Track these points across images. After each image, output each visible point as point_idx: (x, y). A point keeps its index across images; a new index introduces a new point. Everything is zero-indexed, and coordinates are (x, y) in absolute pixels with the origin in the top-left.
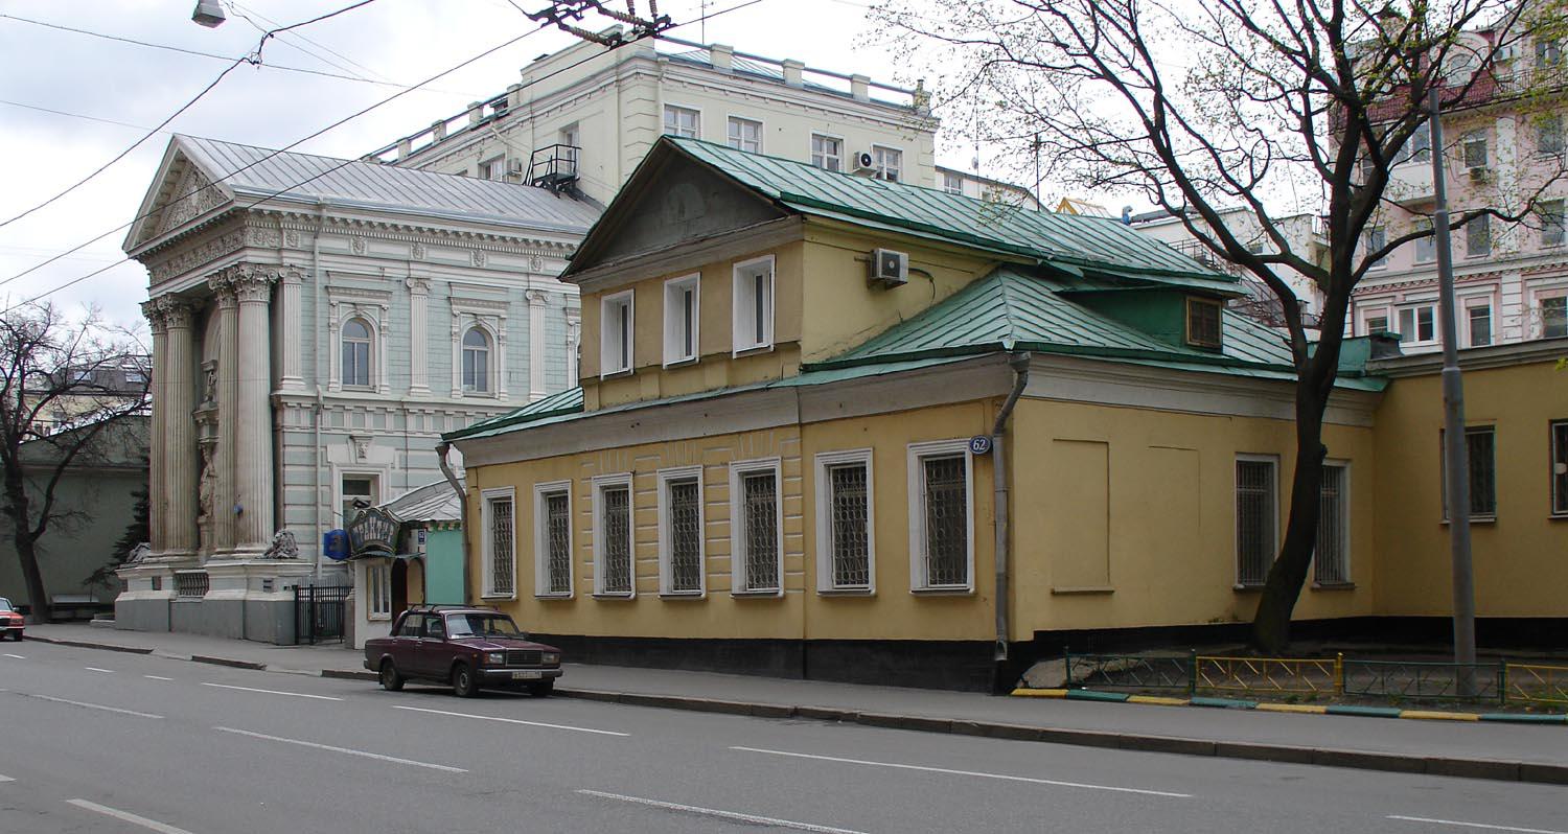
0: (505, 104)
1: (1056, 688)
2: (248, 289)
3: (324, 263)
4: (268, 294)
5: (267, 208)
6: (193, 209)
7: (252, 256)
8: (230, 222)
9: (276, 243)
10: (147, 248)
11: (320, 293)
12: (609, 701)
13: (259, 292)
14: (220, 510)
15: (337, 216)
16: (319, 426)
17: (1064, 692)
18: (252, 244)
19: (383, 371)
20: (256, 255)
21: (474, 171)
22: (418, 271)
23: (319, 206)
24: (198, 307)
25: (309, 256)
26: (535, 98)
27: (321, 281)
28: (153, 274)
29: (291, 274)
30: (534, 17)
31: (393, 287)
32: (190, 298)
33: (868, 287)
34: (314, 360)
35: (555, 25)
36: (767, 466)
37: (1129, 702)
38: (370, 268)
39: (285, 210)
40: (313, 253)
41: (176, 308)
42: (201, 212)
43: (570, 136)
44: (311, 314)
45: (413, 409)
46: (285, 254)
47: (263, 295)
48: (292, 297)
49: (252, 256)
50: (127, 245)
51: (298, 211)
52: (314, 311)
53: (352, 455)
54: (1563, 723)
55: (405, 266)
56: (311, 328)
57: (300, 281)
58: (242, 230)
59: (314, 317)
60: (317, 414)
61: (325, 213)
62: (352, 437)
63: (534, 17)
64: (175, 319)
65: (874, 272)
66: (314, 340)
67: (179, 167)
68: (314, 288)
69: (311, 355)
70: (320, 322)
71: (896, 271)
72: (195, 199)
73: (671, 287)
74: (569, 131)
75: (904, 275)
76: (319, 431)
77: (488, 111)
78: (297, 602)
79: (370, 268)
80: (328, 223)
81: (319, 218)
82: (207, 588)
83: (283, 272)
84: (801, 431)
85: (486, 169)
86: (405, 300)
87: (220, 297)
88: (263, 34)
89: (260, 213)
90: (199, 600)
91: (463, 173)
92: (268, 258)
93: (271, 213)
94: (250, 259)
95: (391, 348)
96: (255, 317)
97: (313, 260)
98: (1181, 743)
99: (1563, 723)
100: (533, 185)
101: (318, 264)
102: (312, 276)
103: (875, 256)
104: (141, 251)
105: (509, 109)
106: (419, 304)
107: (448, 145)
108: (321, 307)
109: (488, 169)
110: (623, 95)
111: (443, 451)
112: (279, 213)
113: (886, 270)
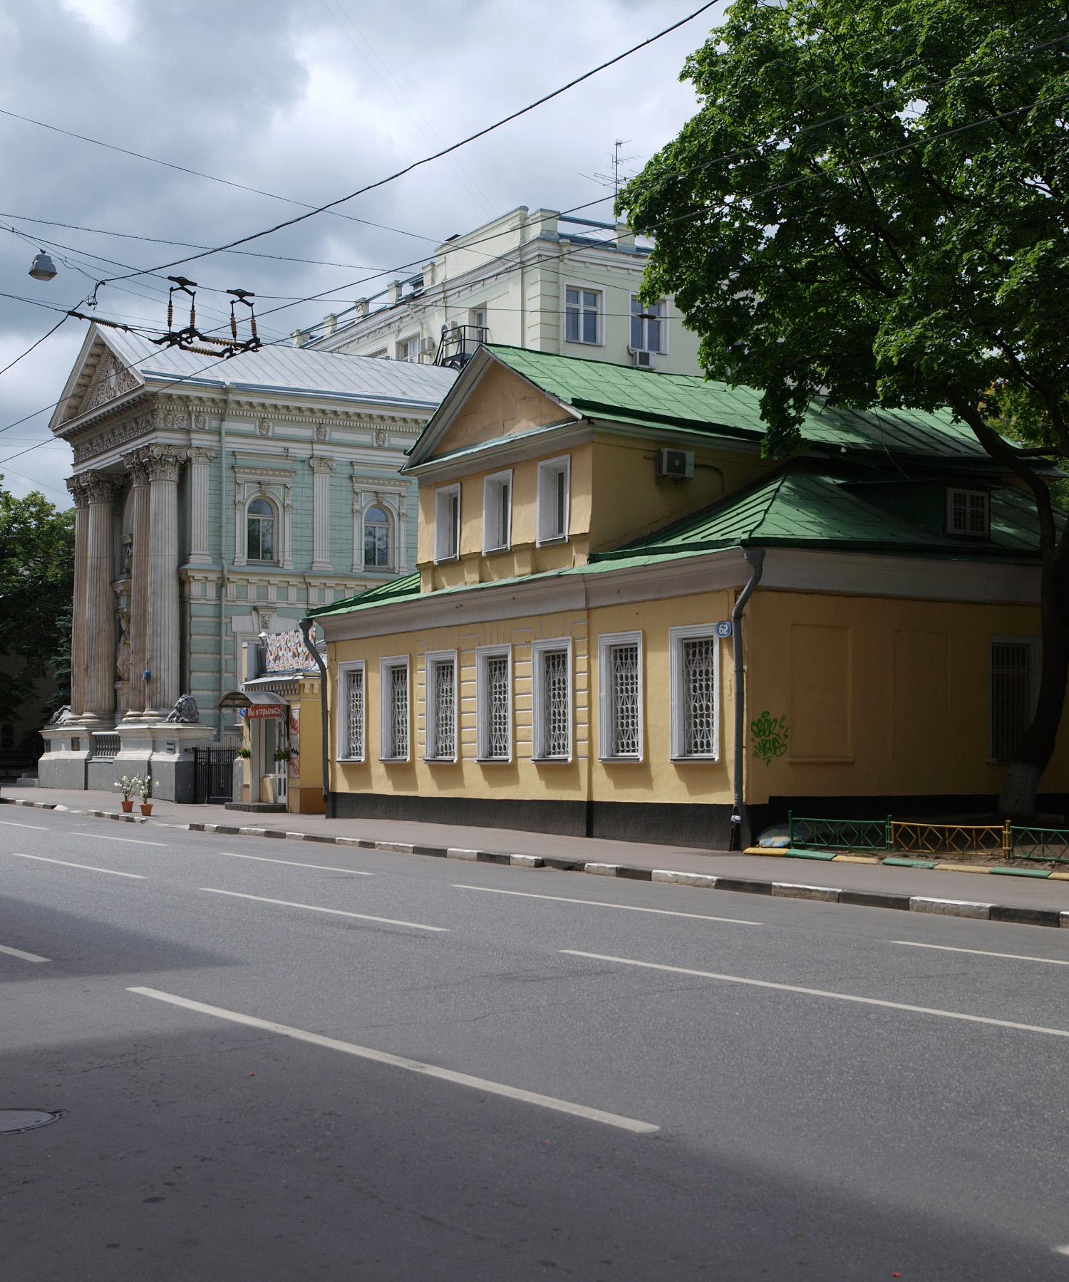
0: (421, 283)
2: (158, 468)
3: (231, 444)
5: (174, 391)
6: (112, 393)
7: (162, 437)
8: (142, 407)
9: (185, 424)
10: (70, 427)
11: (226, 473)
12: (751, 884)
14: (134, 673)
15: (243, 399)
17: (784, 851)
18: (162, 425)
19: (287, 549)
21: (392, 352)
22: (320, 450)
23: (226, 390)
24: (119, 482)
25: (216, 438)
26: (449, 278)
28: (77, 450)
30: (159, 342)
31: (298, 466)
32: (110, 475)
35: (176, 347)
36: (561, 646)
38: (274, 447)
39: (192, 394)
40: (220, 434)
41: (97, 484)
42: (118, 394)
43: (480, 316)
44: (218, 492)
45: (314, 582)
46: (193, 436)
47: (173, 474)
48: (200, 477)
49: (162, 437)
51: (204, 395)
52: (221, 490)
53: (256, 626)
55: (309, 446)
56: (218, 506)
57: (206, 460)
58: (153, 412)
60: (222, 586)
61: (231, 397)
62: (255, 609)
63: (159, 342)
65: (660, 470)
67: (97, 351)
68: (221, 468)
70: (227, 500)
71: (682, 467)
72: (113, 381)
73: (491, 483)
74: (479, 313)
75: (689, 471)
76: (224, 603)
77: (408, 290)
79: (274, 447)
80: (234, 406)
81: (225, 401)
85: (403, 347)
86: (308, 479)
87: (134, 476)
88: (95, 282)
89: (170, 397)
92: (176, 439)
93: (180, 397)
94: (160, 441)
95: (295, 525)
96: (163, 495)
98: (1007, 910)
100: (443, 365)
101: (225, 445)
102: (219, 456)
104: (65, 429)
105: (424, 289)
106: (322, 483)
107: (370, 322)
108: (227, 486)
109: (406, 347)
110: (526, 275)
111: (306, 625)
112: (188, 397)
113: (671, 467)
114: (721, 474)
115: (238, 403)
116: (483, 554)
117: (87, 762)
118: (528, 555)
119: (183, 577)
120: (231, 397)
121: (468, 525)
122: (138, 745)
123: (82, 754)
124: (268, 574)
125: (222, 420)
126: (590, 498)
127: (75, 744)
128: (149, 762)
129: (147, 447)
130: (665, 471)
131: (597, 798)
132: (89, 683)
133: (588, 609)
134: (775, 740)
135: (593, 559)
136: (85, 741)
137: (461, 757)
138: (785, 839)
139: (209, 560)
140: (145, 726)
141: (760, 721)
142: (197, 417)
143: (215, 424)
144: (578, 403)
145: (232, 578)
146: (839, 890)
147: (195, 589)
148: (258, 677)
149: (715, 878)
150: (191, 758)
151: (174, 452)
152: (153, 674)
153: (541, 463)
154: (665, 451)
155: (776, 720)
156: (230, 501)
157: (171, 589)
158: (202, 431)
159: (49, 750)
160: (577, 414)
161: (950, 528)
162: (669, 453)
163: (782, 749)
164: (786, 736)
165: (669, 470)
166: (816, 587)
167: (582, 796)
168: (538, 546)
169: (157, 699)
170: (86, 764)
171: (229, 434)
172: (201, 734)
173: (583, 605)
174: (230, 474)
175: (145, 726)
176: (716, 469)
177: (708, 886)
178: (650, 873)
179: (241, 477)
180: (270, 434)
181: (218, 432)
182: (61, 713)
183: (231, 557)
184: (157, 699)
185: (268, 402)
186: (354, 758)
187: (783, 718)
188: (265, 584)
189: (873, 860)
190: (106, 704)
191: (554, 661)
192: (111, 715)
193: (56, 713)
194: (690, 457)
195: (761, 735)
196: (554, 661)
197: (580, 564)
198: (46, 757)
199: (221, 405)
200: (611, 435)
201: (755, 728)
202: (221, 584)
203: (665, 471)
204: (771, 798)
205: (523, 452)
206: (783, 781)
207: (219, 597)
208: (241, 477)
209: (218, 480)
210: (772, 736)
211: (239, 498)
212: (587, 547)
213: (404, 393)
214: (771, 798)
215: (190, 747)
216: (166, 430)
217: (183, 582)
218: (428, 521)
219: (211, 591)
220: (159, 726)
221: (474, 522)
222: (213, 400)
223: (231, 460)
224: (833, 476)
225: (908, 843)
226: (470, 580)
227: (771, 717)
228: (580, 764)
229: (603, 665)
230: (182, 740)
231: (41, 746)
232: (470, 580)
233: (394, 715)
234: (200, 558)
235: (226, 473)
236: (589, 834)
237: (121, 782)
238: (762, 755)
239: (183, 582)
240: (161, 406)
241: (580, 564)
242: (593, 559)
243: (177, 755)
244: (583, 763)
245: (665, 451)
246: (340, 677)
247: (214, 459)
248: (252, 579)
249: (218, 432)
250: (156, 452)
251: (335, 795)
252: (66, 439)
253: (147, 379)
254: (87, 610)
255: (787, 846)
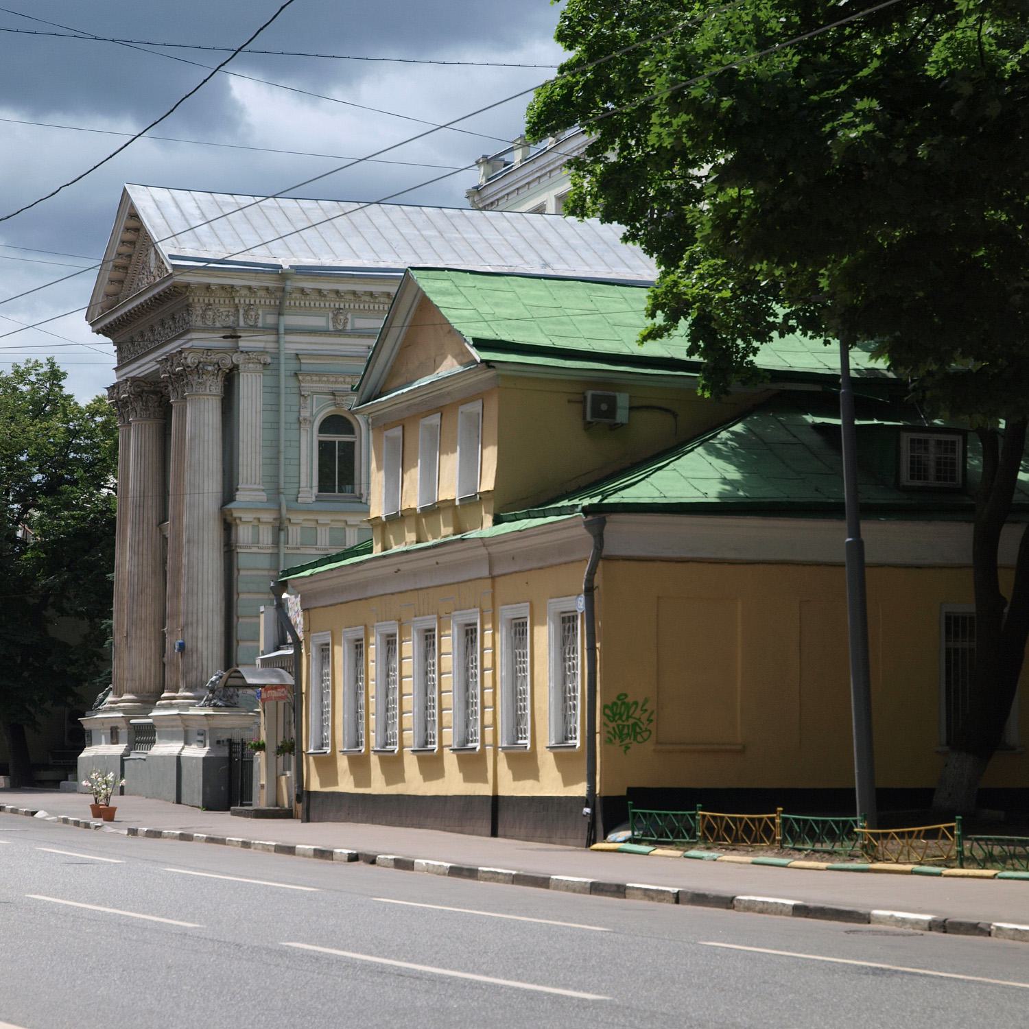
1: (621, 842)
4: (220, 384)
13: (208, 383)
15: (308, 285)
16: (282, 545)
18: (199, 323)
20: (201, 341)
25: (272, 338)
27: (286, 368)
28: (119, 351)
29: (249, 361)
33: (585, 430)
34: (278, 465)
37: (652, 855)
41: (139, 395)
44: (274, 407)
47: (214, 387)
50: (89, 317)
52: (278, 405)
54: (1026, 879)
56: (275, 425)
57: (259, 367)
58: (188, 308)
59: (278, 411)
60: (280, 529)
61: (290, 285)
64: (138, 409)
65: (584, 417)
66: (278, 440)
68: (278, 376)
69: (274, 458)
70: (287, 417)
71: (612, 412)
75: (622, 416)
76: (283, 550)
78: (230, 759)
80: (296, 295)
81: (283, 290)
82: (153, 742)
83: (237, 358)
84: (493, 587)
87: (170, 388)
90: (144, 757)
91: (540, 210)
92: (213, 340)
93: (223, 287)
94: (196, 343)
97: (278, 342)
99: (1026, 879)
101: (283, 346)
103: (585, 398)
104: (107, 321)
112: (232, 287)
113: (596, 412)
114: (675, 415)
115: (302, 291)
116: (418, 511)
117: (123, 759)
118: (450, 514)
119: (229, 519)
120: (290, 285)
121: (408, 473)
122: (171, 737)
123: (119, 749)
124: (343, 512)
125: (280, 314)
126: (496, 448)
127: (114, 738)
128: (179, 758)
129: (181, 352)
130: (589, 418)
131: (501, 793)
132: (130, 655)
133: (493, 578)
134: (635, 724)
135: (497, 521)
136: (123, 733)
137: (441, 747)
138: (628, 834)
139: (263, 496)
140: (175, 712)
141: (614, 704)
142: (246, 312)
143: (271, 320)
144: (480, 344)
145: (296, 518)
146: (514, 872)
147: (243, 534)
148: (278, 649)
149: (448, 865)
150: (225, 752)
151: (215, 358)
152: (188, 645)
153: (462, 408)
154: (589, 394)
155: (636, 703)
156: (292, 417)
157: (212, 535)
158: (254, 328)
159: (91, 745)
160: (478, 355)
161: (905, 478)
162: (593, 396)
163: (645, 735)
164: (650, 721)
165: (593, 415)
166: (690, 555)
167: (485, 790)
168: (457, 503)
169: (193, 676)
170: (122, 761)
171: (291, 331)
172: (230, 721)
173: (486, 573)
174: (293, 382)
175: (175, 712)
176: (667, 410)
177: (781, 913)
178: (413, 863)
179: (308, 386)
180: (349, 327)
181: (275, 329)
182: (106, 695)
183: (294, 491)
184: (193, 676)
185: (342, 287)
186: (389, 748)
187: (646, 700)
188: (313, 524)
189: (679, 853)
190: (151, 684)
191: (469, 633)
192: (149, 699)
193: (101, 696)
194: (623, 400)
195: (618, 718)
196: (469, 633)
197: (488, 529)
198: (88, 753)
199: (279, 294)
200: (529, 378)
201: (608, 712)
202: (279, 528)
203: (589, 418)
204: (628, 789)
205: (449, 393)
206: (645, 768)
207: (276, 543)
208: (308, 386)
209: (274, 391)
210: (631, 721)
211: (305, 413)
212: (492, 506)
213: (546, 265)
214: (628, 789)
215: (225, 737)
216: (204, 330)
217: (228, 526)
218: (379, 469)
219: (266, 536)
220: (192, 712)
221: (413, 470)
222: (267, 289)
223: (293, 366)
224: (814, 414)
225: (717, 836)
226: (409, 540)
227: (630, 700)
228: (487, 751)
229: (504, 637)
230: (213, 730)
231: (81, 739)
232: (409, 540)
233: (357, 696)
234: (250, 491)
235: (285, 382)
236: (494, 834)
237: (91, 781)
238: (617, 741)
239: (228, 526)
240: (198, 302)
241: (488, 529)
242: (497, 521)
243: (207, 748)
244: (489, 750)
245: (589, 394)
246: (313, 651)
247: (270, 365)
248: (323, 519)
249: (275, 329)
250: (191, 359)
251: (309, 793)
252: (106, 335)
253: (174, 266)
254: (128, 563)
255: (632, 840)
